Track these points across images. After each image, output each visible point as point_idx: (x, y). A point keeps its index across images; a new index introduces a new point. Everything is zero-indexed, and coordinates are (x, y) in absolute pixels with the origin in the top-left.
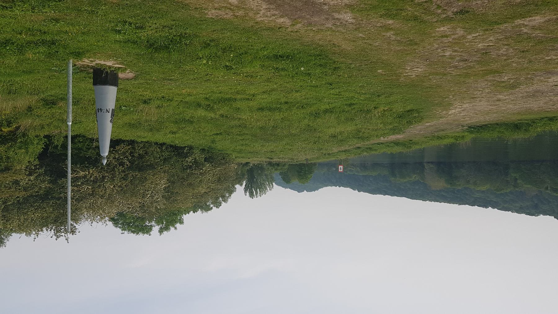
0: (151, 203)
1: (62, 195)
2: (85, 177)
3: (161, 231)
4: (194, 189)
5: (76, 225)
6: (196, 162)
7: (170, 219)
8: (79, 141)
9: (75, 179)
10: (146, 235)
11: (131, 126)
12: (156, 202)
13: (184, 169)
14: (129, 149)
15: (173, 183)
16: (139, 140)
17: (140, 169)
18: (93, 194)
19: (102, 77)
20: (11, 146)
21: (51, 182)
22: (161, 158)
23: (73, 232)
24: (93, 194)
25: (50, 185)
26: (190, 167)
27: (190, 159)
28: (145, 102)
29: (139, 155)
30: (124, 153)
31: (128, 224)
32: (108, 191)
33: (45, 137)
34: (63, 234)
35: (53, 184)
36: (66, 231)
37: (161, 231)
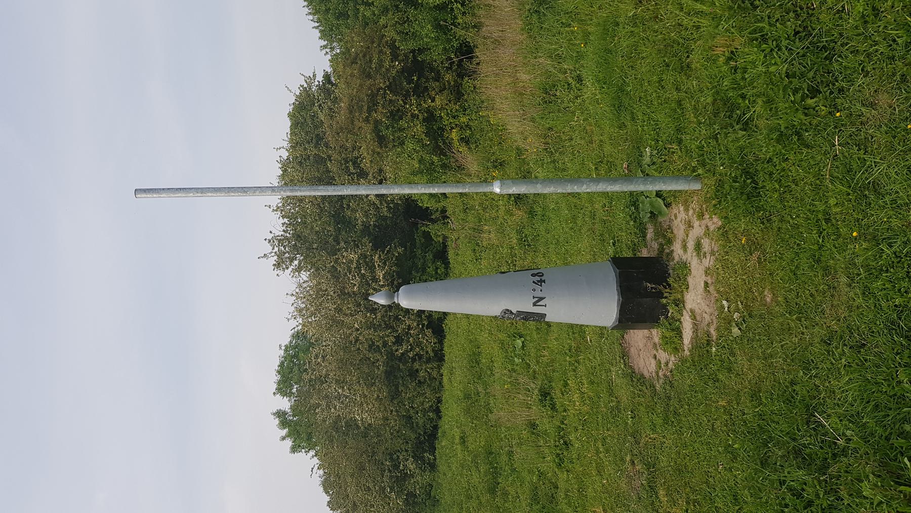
0: (327, 396)
1: (342, 244)
2: (375, 280)
3: (280, 414)
4: (352, 476)
5: (290, 269)
6: (405, 476)
7: (300, 429)
8: (437, 268)
9: (370, 264)
10: (275, 386)
11: (475, 359)
12: (328, 406)
13: (391, 455)
14: (427, 352)
15: (365, 436)
16: (445, 371)
17: (390, 374)
18: (345, 294)
19: (645, 287)
20: (424, 146)
21: (366, 227)
22: (412, 411)
23: (278, 265)
24: (345, 294)
25: (359, 227)
26: (396, 467)
27: (411, 465)
28: (545, 394)
29: (417, 371)
30: (419, 344)
31: (296, 356)
32: (348, 320)
33: (444, 211)
34: (276, 249)
35: (362, 231)
36: (280, 255)
37: (280, 414)
